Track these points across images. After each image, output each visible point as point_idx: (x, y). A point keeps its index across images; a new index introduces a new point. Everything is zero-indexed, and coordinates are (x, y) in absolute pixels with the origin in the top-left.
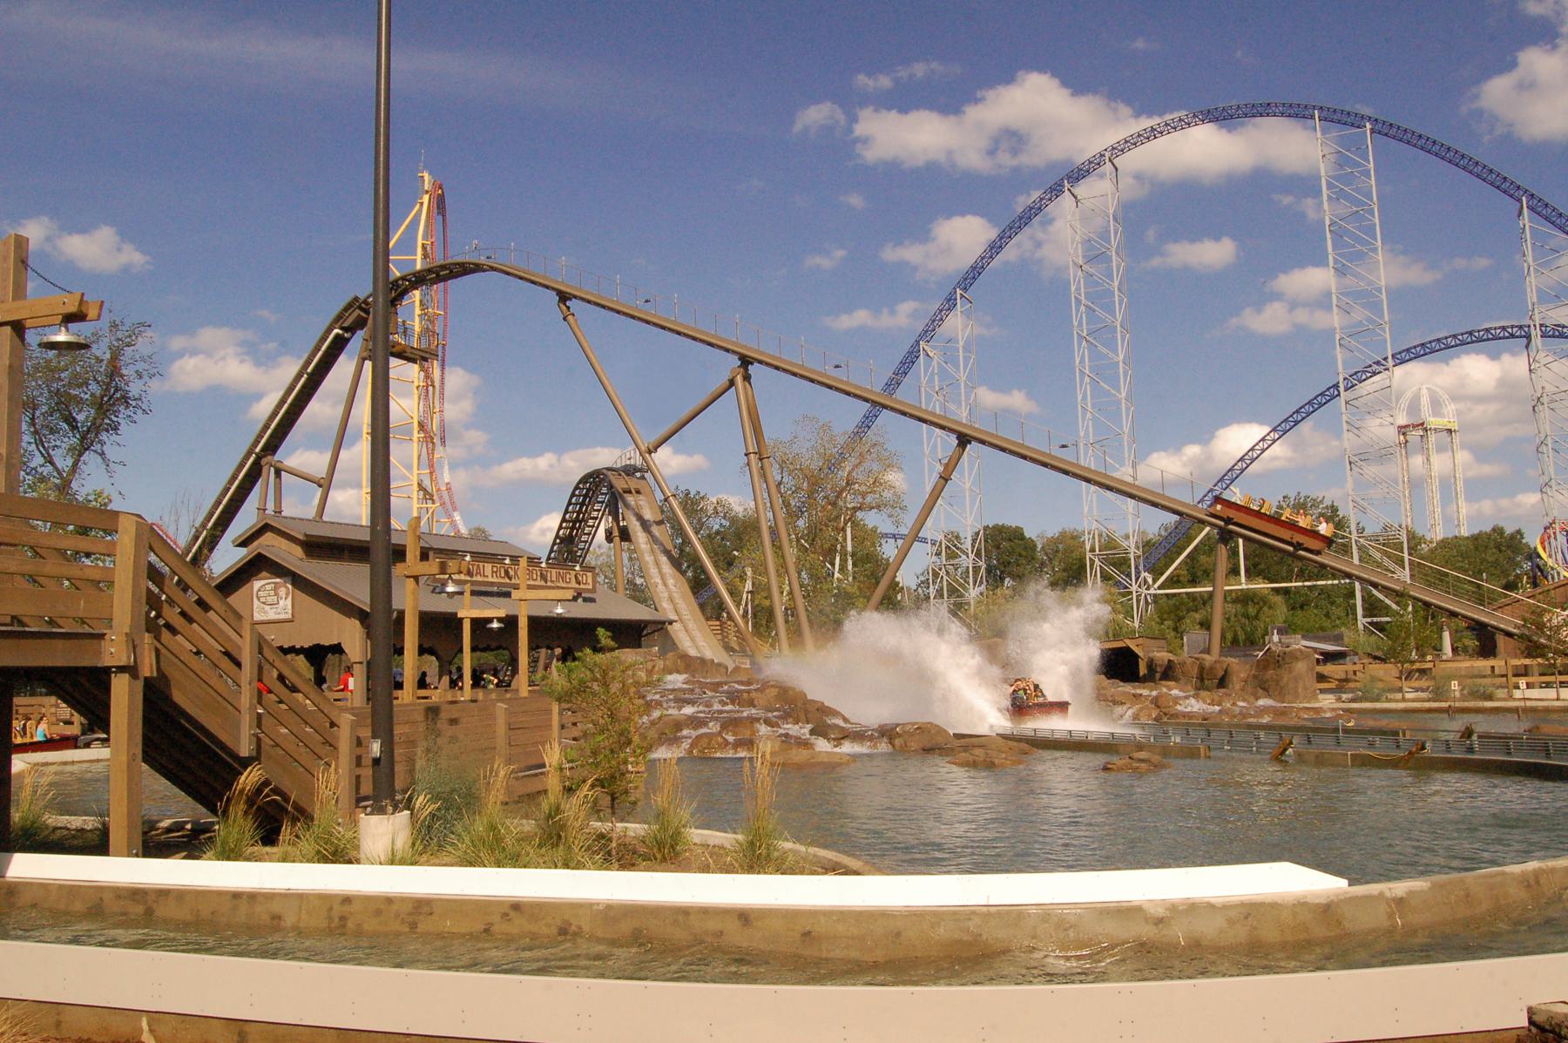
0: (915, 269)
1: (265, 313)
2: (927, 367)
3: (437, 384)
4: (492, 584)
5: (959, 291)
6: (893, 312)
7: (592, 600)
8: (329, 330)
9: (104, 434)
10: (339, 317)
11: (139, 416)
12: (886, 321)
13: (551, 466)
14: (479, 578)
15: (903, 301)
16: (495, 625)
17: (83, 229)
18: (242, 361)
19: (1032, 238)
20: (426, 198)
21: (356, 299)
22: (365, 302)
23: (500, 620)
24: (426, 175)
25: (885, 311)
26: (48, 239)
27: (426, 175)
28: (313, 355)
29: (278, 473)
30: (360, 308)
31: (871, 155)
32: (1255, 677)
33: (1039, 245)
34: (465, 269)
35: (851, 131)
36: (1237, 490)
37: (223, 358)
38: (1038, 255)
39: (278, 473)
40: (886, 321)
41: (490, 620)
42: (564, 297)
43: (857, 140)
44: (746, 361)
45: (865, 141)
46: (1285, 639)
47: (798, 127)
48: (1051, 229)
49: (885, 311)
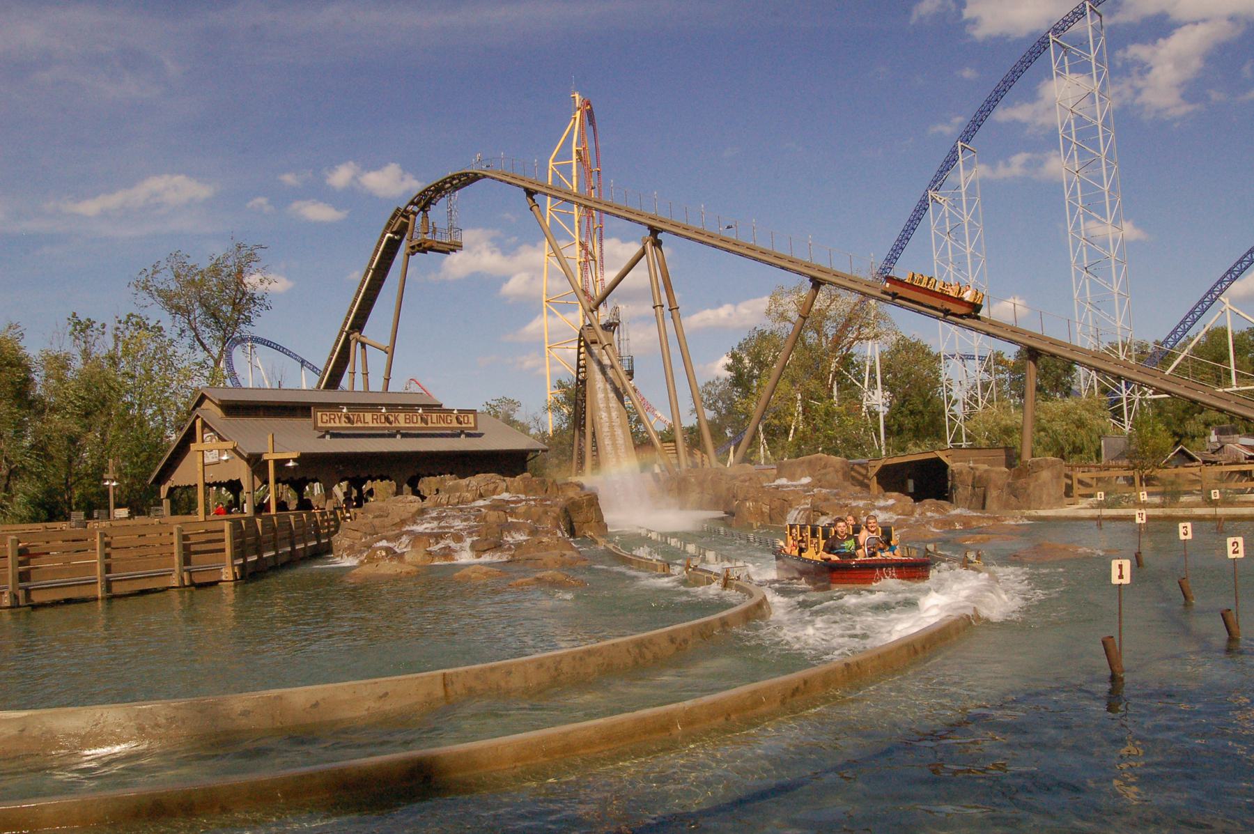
0: (1024, 126)
1: (507, 215)
2: (936, 213)
3: (597, 259)
4: (373, 428)
5: (960, 144)
6: (1007, 165)
7: (480, 435)
8: (384, 235)
9: (242, 326)
10: (389, 225)
11: (264, 313)
12: (1002, 172)
13: (730, 315)
14: (359, 425)
15: (1017, 153)
16: (291, 464)
17: (377, 167)
18: (493, 252)
19: (1131, 87)
20: (578, 113)
21: (398, 209)
22: (405, 210)
23: (294, 460)
24: (577, 95)
25: (1001, 163)
26: (354, 178)
27: (577, 95)
28: (375, 254)
29: (363, 345)
30: (402, 215)
31: (980, 33)
32: (1009, 485)
33: (1138, 92)
34: (468, 179)
35: (960, 15)
36: (1226, 301)
37: (479, 252)
38: (1138, 101)
39: (363, 345)
40: (1002, 172)
41: (288, 460)
42: (530, 193)
43: (967, 22)
44: (654, 231)
45: (974, 22)
46: (1223, 439)
47: (914, 19)
48: (1150, 76)
49: (1001, 163)
